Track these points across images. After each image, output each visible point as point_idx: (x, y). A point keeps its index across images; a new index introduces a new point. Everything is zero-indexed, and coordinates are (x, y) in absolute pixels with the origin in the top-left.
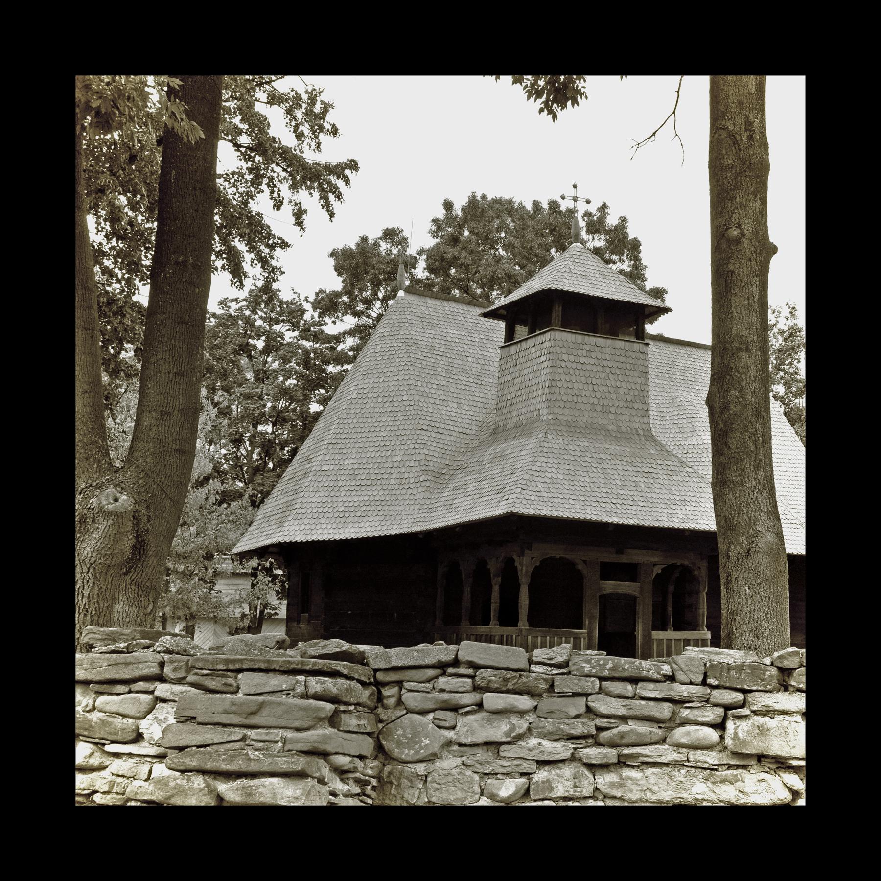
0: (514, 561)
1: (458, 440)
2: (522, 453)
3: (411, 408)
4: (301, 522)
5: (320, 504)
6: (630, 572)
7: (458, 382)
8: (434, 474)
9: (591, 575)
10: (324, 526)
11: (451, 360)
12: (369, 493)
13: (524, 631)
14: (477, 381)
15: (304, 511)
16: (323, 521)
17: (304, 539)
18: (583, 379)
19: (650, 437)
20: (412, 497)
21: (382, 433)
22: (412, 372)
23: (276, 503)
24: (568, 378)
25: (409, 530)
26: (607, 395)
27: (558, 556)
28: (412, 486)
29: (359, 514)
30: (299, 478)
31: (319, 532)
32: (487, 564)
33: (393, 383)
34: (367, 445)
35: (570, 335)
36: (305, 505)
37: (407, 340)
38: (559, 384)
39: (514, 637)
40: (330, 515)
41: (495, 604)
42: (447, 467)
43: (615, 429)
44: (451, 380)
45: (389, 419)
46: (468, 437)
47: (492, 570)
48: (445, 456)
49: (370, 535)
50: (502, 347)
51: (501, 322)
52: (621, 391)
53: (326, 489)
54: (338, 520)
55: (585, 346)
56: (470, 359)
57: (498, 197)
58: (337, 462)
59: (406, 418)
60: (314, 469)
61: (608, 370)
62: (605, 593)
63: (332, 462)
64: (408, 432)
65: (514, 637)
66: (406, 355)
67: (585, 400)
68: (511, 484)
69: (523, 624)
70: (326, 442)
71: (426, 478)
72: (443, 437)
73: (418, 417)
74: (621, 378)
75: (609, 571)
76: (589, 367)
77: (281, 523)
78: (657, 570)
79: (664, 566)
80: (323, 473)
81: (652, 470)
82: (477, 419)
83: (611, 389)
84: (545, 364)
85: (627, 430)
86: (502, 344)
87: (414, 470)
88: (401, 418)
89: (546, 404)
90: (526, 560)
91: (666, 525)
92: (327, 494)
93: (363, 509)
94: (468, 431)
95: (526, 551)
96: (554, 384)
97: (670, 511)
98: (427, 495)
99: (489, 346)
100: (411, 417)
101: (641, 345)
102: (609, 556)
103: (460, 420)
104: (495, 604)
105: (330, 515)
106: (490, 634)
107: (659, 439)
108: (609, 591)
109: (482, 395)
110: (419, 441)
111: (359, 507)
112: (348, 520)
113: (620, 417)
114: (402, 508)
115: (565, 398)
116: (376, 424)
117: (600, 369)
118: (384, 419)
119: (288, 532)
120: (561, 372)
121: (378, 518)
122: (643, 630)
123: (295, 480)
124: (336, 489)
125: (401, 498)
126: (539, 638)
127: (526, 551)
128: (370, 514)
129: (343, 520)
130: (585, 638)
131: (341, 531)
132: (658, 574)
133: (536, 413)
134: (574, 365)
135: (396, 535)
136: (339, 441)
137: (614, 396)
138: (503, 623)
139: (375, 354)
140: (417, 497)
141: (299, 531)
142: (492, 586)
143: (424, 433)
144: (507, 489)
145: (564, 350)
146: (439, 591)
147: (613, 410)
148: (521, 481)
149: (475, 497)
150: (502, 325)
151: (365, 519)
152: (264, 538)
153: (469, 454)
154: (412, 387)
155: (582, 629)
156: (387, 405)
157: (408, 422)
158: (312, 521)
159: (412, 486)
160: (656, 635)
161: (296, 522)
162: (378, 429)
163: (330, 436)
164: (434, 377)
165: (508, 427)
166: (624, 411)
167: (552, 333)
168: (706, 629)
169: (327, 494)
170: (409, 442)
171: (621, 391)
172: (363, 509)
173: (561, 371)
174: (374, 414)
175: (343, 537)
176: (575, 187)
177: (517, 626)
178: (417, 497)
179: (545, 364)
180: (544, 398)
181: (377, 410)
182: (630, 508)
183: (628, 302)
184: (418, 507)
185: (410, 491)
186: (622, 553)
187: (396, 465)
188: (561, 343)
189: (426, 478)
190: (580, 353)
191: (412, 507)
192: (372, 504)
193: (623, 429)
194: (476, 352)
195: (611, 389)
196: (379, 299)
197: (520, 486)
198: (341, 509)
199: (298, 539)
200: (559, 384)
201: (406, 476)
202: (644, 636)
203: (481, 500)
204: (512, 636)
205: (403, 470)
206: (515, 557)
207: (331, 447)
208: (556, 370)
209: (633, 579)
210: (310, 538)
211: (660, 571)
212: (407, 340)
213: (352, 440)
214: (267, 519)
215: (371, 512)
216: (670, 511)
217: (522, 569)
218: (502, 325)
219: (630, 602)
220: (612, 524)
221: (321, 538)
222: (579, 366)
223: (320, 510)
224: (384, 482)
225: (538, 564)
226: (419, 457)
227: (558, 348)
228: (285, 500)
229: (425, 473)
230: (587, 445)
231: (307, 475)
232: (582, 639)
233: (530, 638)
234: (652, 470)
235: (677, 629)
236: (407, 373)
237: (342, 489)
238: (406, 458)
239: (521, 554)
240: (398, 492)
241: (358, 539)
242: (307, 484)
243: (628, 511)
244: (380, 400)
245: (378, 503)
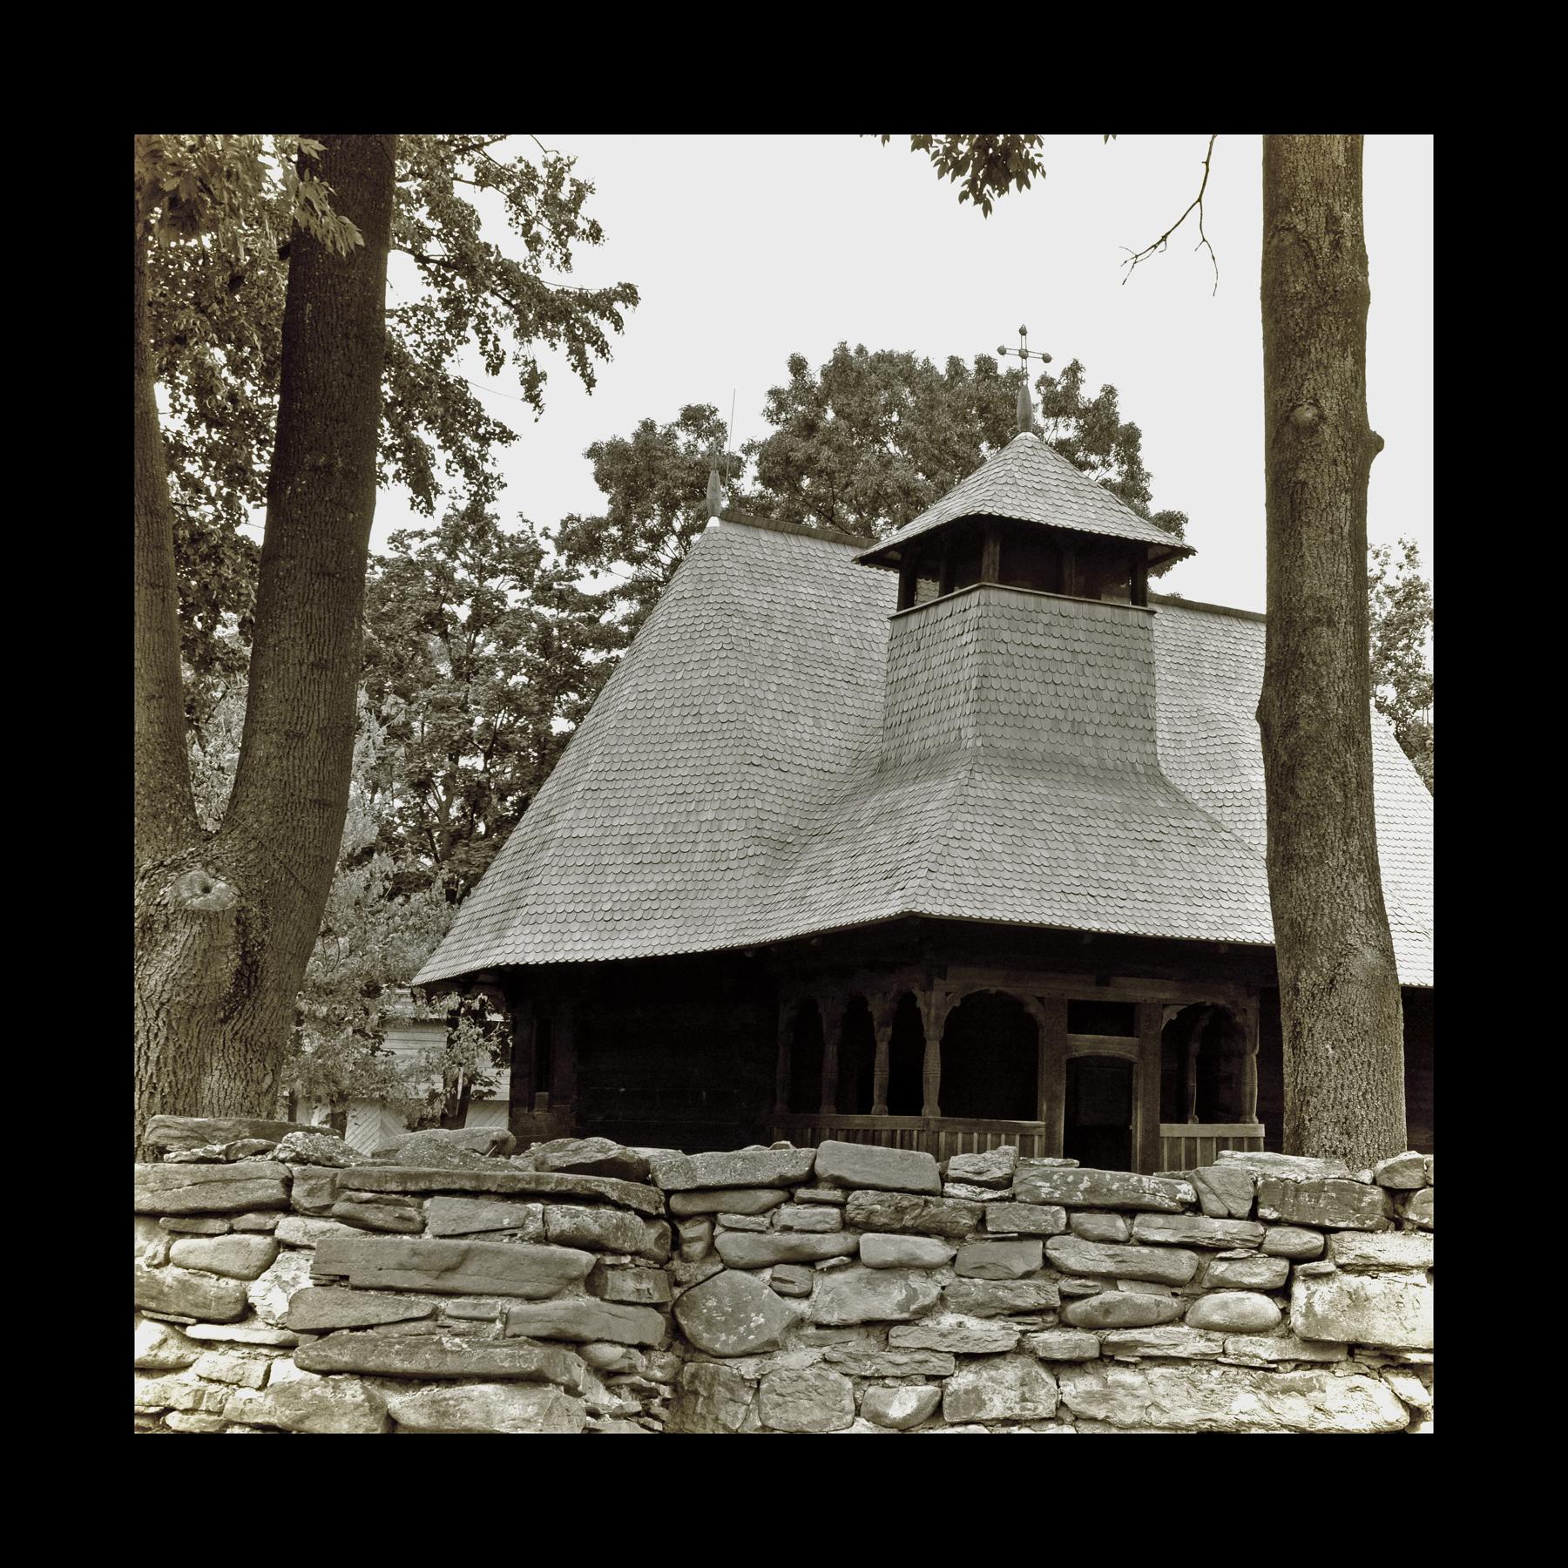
0: (914, 998)
1: (816, 783)
2: (929, 807)
3: (732, 726)
4: (536, 928)
5: (570, 898)
6: (1121, 1018)
7: (816, 679)
8: (772, 844)
9: (1051, 1024)
10: (577, 936)
11: (802, 641)
12: (658, 878)
13: (932, 1123)
14: (850, 678)
15: (540, 909)
16: (574, 926)
17: (541, 959)
18: (1038, 675)
19: (1156, 778)
20: (733, 885)
21: (680, 771)
22: (734, 663)
23: (492, 895)
24: (1010, 672)
25: (729, 944)
26: (1081, 703)
27: (993, 990)
28: (734, 865)
29: (638, 915)
30: (532, 851)
31: (568, 946)
32: (866, 1004)
33: (699, 682)
34: (653, 792)
35: (1014, 596)
36: (542, 899)
37: (724, 606)
38: (995, 683)
39: (915, 1133)
40: (587, 917)
41: (881, 1075)
42: (795, 831)
43: (1095, 763)
44: (803, 677)
45: (692, 746)
46: (832, 777)
47: (876, 1015)
48: (792, 812)
49: (659, 952)
50: (893, 618)
51: (891, 573)
52: (1106, 695)
53: (580, 870)
54: (602, 926)
55: (1041, 616)
56: (836, 640)
57: (887, 350)
58: (599, 822)
59: (722, 744)
60: (558, 835)
61: (1082, 659)
62: (1077, 1055)
63: (591, 823)
64: (727, 769)
65: (915, 1133)
66: (723, 632)
67: (1040, 712)
68: (910, 861)
69: (931, 1110)
70: (580, 787)
71: (759, 850)
72: (789, 777)
73: (744, 742)
75: (1084, 1017)
76: (1048, 654)
77: (500, 931)
78: (1170, 1014)
79: (1181, 1008)
80: (575, 842)
81: (1160, 837)
82: (850, 745)
83: (1088, 693)
84: (971, 648)
85: (1116, 765)
86: (894, 613)
87: (737, 836)
88: (714, 744)
89: (972, 720)
90: (936, 997)
91: (1185, 934)
92: (581, 879)
93: (646, 905)
94: (834, 768)
95: (937, 981)
98: (761, 881)
99: (870, 615)
100: (731, 742)
101: (1140, 613)
102: (1083, 990)
103: (818, 747)
104: (881, 1075)
105: (587, 917)
106: (871, 1128)
107: (1173, 781)
108: (1085, 1052)
109: (858, 703)
110: (745, 785)
111: (638, 903)
112: (619, 926)
113: (1103, 742)
114: (715, 904)
115: (1005, 709)
116: (669, 755)
117: (1067, 657)
118: (683, 746)
119: (513, 947)
120: (999, 663)
121: (672, 922)
122: (1145, 1122)
123: (524, 853)
124: (599, 870)
125: (713, 885)
126: (960, 1135)
127: (937, 981)
128: (658, 914)
129: (610, 926)
130: (1040, 1136)
131: (607, 945)
132: (1170, 1021)
133: (953, 735)
134: (1021, 650)
135: (705, 953)
136: (604, 785)
137: (1092, 705)
138: (895, 1109)
139: (667, 631)
140: (742, 884)
141: (531, 946)
142: (875, 1043)
143: (754, 770)
144: (903, 870)
145: (1004, 623)
146: (781, 1051)
147: (1091, 729)
148: (927, 857)
149: (846, 884)
150: (894, 578)
151: (649, 924)
152: (470, 957)
153: (834, 808)
154: (733, 689)
155: (1035, 1119)
156: (688, 720)
157: (727, 751)
158: (555, 928)
159: (734, 865)
160: (1168, 1130)
161: (527, 929)
162: (672, 764)
163: (587, 777)
164: (772, 671)
165: (904, 759)
167: (983, 592)
168: (1256, 1120)
169: (581, 879)
170: (727, 787)
171: (1106, 695)
172: (646, 905)
173: (998, 660)
174: (666, 738)
175: (610, 955)
176: (1023, 332)
177: (920, 1114)
178: (742, 884)
179: (971, 648)
180: (968, 708)
181: (671, 730)
182: (1122, 903)
183: (1118, 538)
185: (729, 875)
186: (1108, 985)
187: (705, 827)
189: (759, 850)
190: (1031, 627)
191: (733, 903)
192: (663, 897)
193: (1109, 763)
194: (846, 627)
195: (1088, 693)
196: (674, 532)
197: (925, 864)
198: (607, 907)
199: (531, 959)
200: (995, 683)
201: (723, 846)
202: (1146, 1132)
203: (856, 889)
204: (911, 1132)
205: (717, 837)
206: (916, 992)
207: (589, 795)
208: (989, 658)
209: (1127, 1031)
210: (551, 958)
211: (1174, 1017)
212: (724, 606)
213: (627, 784)
214: (475, 924)
215: (660, 911)
216: (1193, 910)
217: (929, 1013)
218: (894, 578)
219: (1122, 1072)
220: (1089, 932)
221: (571, 958)
222: (1031, 652)
223: (570, 908)
224: (683, 858)
225: (957, 1004)
226: (746, 813)
227: (993, 619)
228: (508, 889)
229: (757, 841)
230: (1044, 791)
231: (546, 846)
232: (1036, 1138)
233: (943, 1135)
234: (1160, 837)
235: (1205, 1119)
236: (724, 663)
237: (609, 870)
238: (723, 815)
239: (928, 987)
240: (709, 876)
241: (636, 959)
242: (546, 861)
243: (1118, 910)
244: (676, 712)
245: (672, 896)
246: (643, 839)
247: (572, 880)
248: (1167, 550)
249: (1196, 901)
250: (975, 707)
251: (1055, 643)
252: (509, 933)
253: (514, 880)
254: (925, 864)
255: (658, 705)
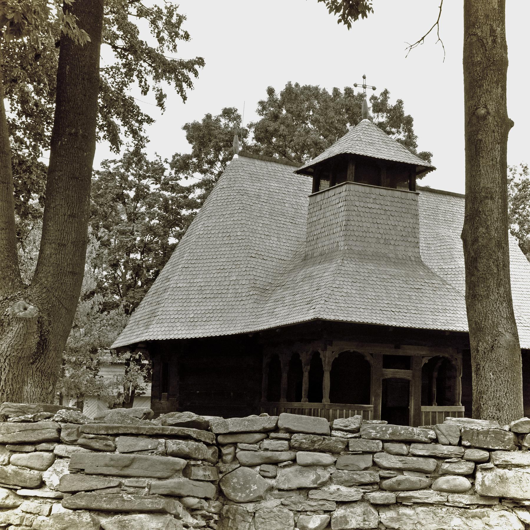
1: (278, 265)
3: (243, 241)
4: (162, 325)
5: (176, 312)
7: (278, 221)
8: (260, 290)
9: (376, 364)
10: (179, 328)
11: (272, 206)
12: (212, 304)
15: (164, 317)
16: (178, 324)
18: (370, 220)
19: (420, 262)
20: (244, 307)
21: (222, 260)
22: (244, 215)
23: (144, 311)
25: (242, 331)
28: (244, 298)
29: (205, 319)
30: (161, 293)
34: (211, 268)
35: (360, 187)
38: (353, 223)
39: (319, 410)
40: (183, 320)
43: (394, 256)
45: (227, 249)
47: (303, 361)
49: (213, 335)
52: (399, 228)
53: (180, 301)
54: (189, 324)
55: (372, 195)
56: (287, 205)
58: (188, 281)
61: (388, 213)
63: (185, 281)
64: (241, 259)
65: (319, 410)
66: (240, 202)
67: (371, 235)
68: (317, 297)
69: (326, 400)
70: (180, 266)
72: (267, 262)
73: (248, 248)
74: (398, 219)
76: (375, 211)
78: (425, 361)
80: (178, 289)
81: (421, 287)
82: (292, 249)
83: (391, 227)
84: (343, 209)
85: (403, 257)
86: (311, 194)
87: (245, 287)
88: (236, 249)
89: (343, 238)
90: (328, 353)
93: (208, 315)
94: (286, 258)
95: (328, 347)
96: (349, 223)
97: (435, 317)
98: (255, 305)
99: (301, 195)
100: (243, 248)
101: (413, 194)
102: (390, 351)
103: (279, 250)
105: (183, 320)
108: (390, 376)
111: (204, 315)
112: (197, 324)
113: (397, 248)
114: (236, 315)
116: (217, 253)
121: (219, 322)
122: (415, 405)
123: (157, 294)
125: (235, 307)
126: (338, 411)
127: (328, 347)
129: (193, 324)
130: (371, 411)
131: (192, 332)
133: (335, 245)
134: (363, 209)
136: (190, 266)
137: (393, 232)
143: (252, 259)
144: (314, 301)
146: (264, 376)
147: (392, 242)
148: (324, 295)
149: (291, 307)
150: (311, 179)
151: (209, 323)
152: (135, 337)
153: (286, 275)
154: (244, 225)
156: (225, 239)
158: (170, 325)
159: (244, 298)
164: (260, 218)
165: (315, 255)
166: (400, 243)
167: (348, 185)
168: (461, 404)
171: (399, 228)
172: (208, 315)
173: (354, 213)
174: (216, 246)
176: (364, 77)
177: (321, 402)
180: (341, 233)
181: (218, 243)
182: (405, 315)
184: (248, 314)
185: (242, 303)
187: (232, 283)
188: (354, 193)
190: (368, 200)
191: (244, 315)
193: (400, 256)
195: (391, 227)
197: (323, 298)
198: (191, 316)
201: (240, 291)
202: (415, 410)
203: (295, 309)
205: (237, 287)
206: (320, 351)
208: (350, 213)
209: (408, 367)
211: (427, 362)
213: (200, 265)
216: (435, 317)
217: (325, 360)
218: (311, 179)
219: (405, 384)
222: (367, 210)
223: (176, 316)
224: (223, 296)
225: (337, 356)
227: (352, 197)
230: (373, 268)
231: (166, 291)
232: (370, 412)
233: (331, 410)
236: (240, 215)
238: (240, 278)
239: (325, 349)
240: (234, 303)
241: (204, 338)
242: (166, 297)
244: (220, 235)
245: (219, 312)
246: (206, 288)
247: (177, 305)
248: (424, 168)
249: (436, 313)
250: (344, 233)
251: (377, 207)
252: (151, 327)
253: (153, 305)
254: (323, 298)
255: (213, 232)
